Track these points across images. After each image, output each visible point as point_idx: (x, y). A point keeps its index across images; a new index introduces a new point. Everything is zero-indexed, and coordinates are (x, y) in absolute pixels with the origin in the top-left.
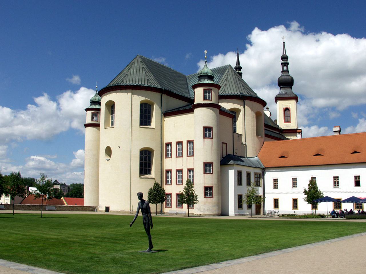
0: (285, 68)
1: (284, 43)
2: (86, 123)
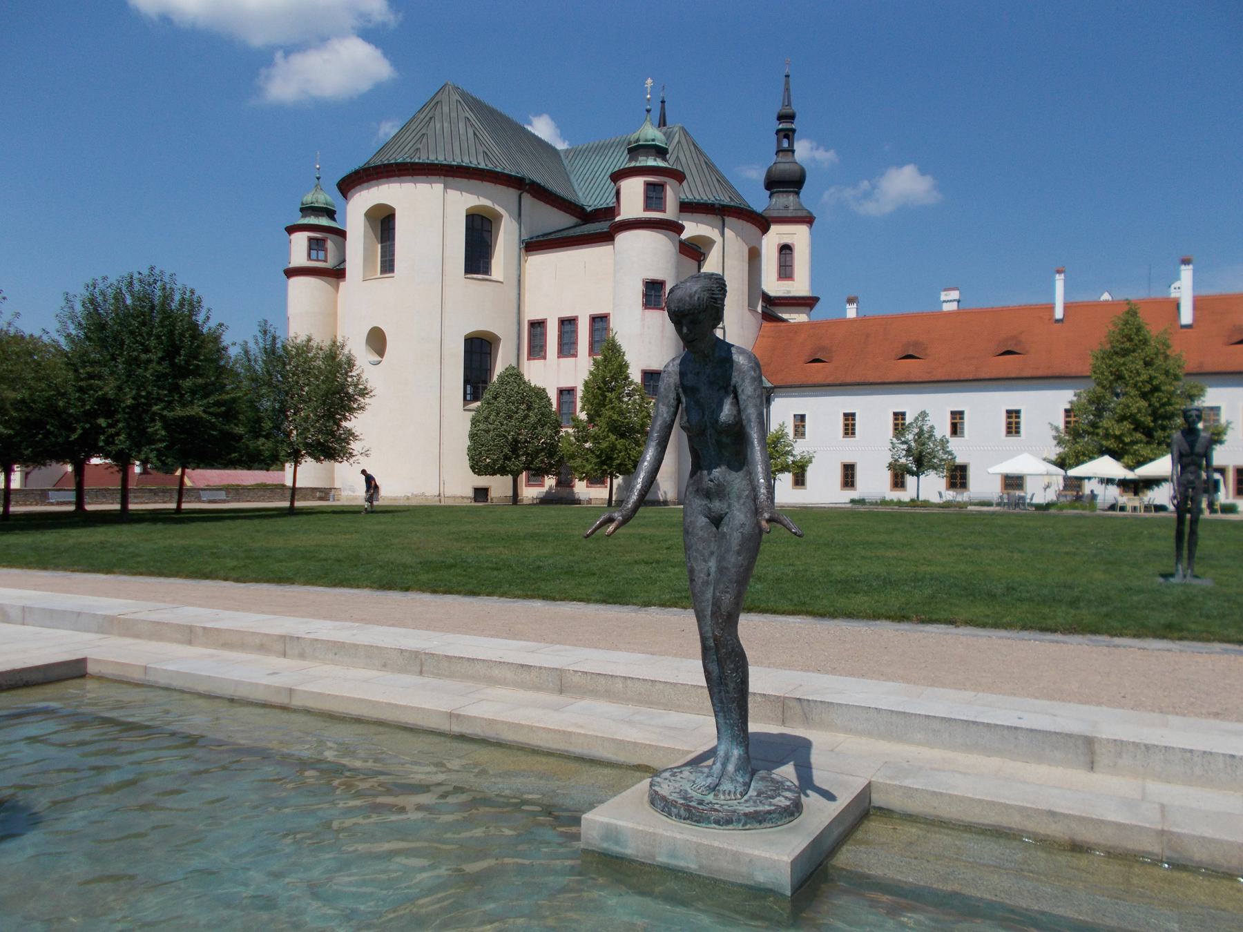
0: (785, 144)
1: (663, 102)
2: (291, 266)
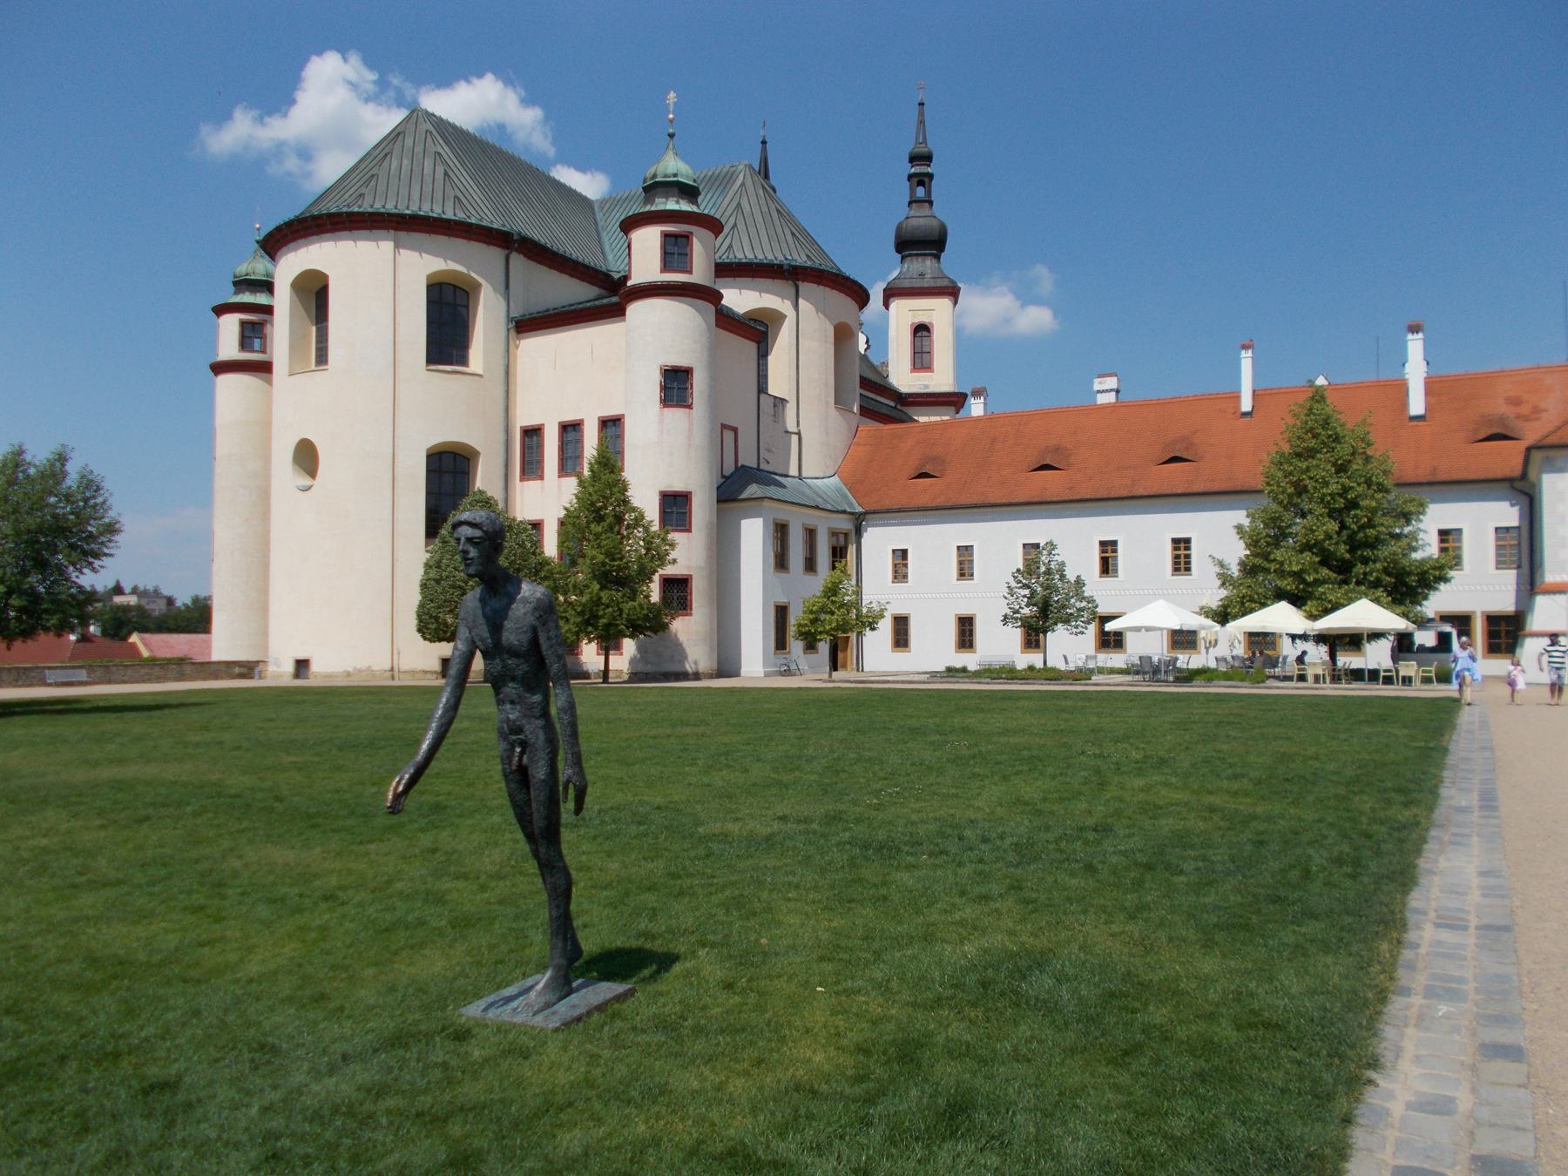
0: (920, 192)
1: (764, 142)
